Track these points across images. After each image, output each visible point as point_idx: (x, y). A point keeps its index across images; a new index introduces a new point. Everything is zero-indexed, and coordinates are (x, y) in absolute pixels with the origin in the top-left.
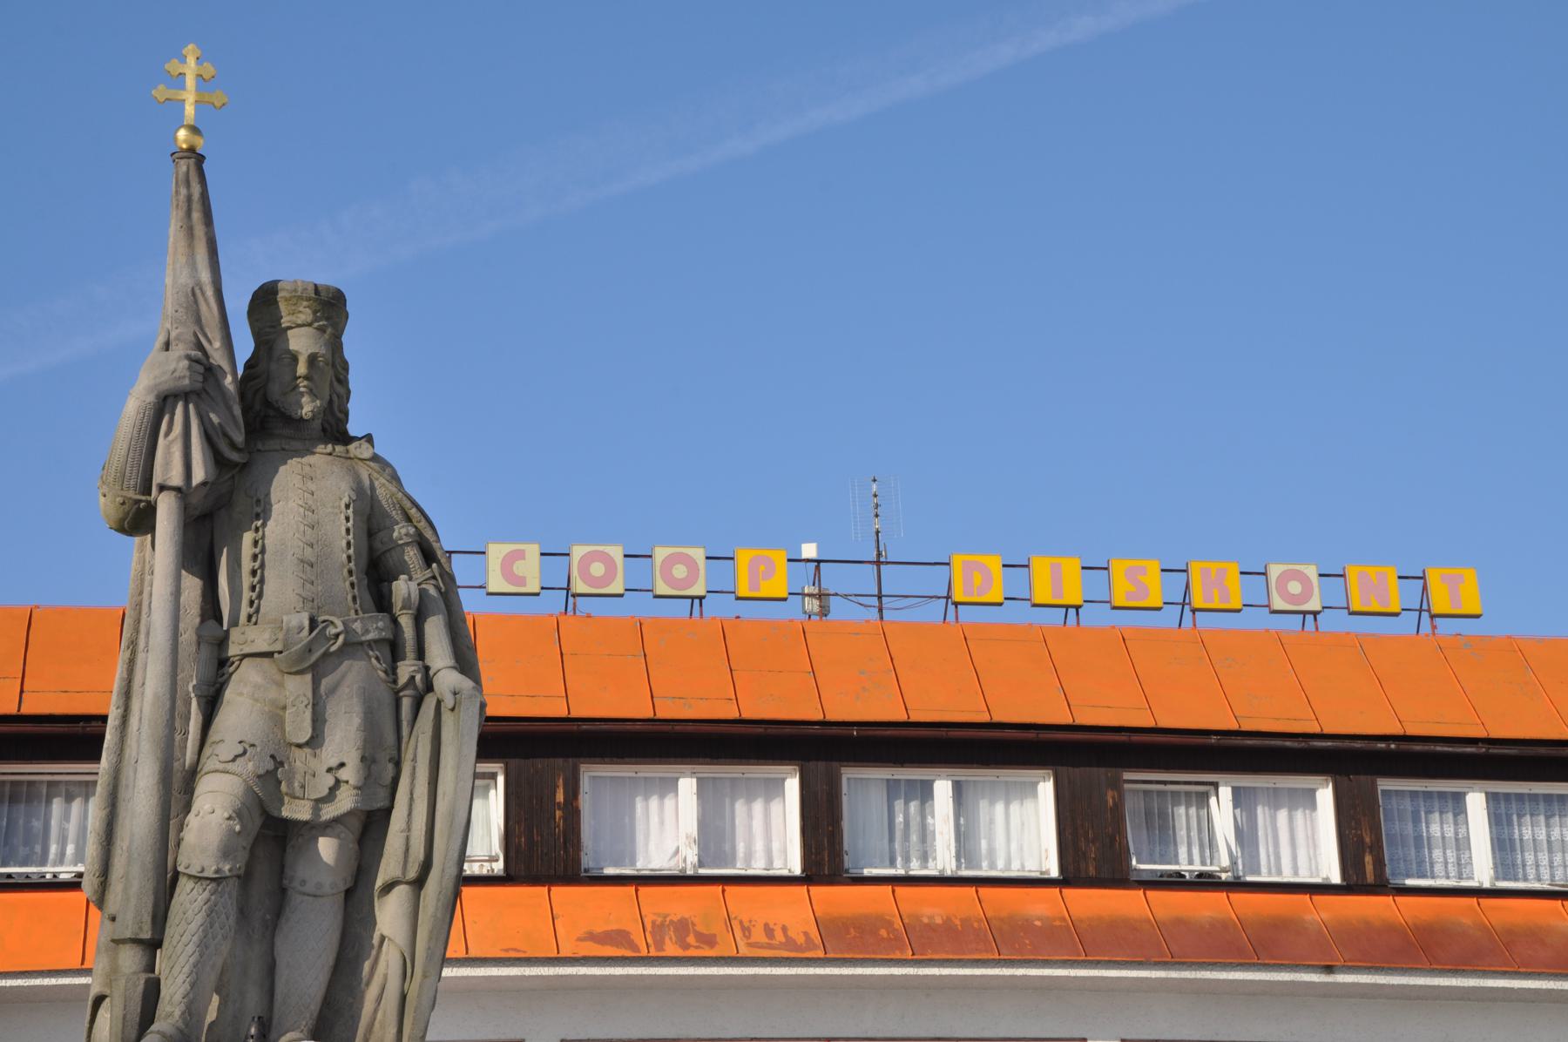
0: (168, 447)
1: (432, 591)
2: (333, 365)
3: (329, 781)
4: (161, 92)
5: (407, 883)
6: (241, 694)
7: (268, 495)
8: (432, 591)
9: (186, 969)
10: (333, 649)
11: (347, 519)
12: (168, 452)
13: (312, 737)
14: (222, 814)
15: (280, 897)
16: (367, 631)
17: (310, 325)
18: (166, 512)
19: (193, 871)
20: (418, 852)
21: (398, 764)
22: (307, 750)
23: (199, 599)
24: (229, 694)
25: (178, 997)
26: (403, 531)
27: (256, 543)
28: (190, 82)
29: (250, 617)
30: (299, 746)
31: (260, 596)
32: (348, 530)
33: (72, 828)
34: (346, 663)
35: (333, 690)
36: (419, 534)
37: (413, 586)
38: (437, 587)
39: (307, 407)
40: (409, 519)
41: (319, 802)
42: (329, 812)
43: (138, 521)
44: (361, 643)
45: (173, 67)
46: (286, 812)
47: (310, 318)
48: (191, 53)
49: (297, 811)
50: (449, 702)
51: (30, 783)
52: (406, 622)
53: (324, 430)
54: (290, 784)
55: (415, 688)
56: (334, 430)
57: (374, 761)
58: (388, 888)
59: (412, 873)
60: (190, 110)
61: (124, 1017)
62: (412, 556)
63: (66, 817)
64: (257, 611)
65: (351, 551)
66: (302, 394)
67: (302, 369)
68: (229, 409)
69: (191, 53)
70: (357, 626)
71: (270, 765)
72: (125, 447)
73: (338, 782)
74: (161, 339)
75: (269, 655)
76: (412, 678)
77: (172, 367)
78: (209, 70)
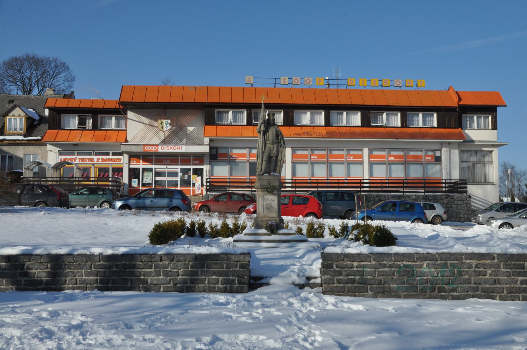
49: (272, 155)
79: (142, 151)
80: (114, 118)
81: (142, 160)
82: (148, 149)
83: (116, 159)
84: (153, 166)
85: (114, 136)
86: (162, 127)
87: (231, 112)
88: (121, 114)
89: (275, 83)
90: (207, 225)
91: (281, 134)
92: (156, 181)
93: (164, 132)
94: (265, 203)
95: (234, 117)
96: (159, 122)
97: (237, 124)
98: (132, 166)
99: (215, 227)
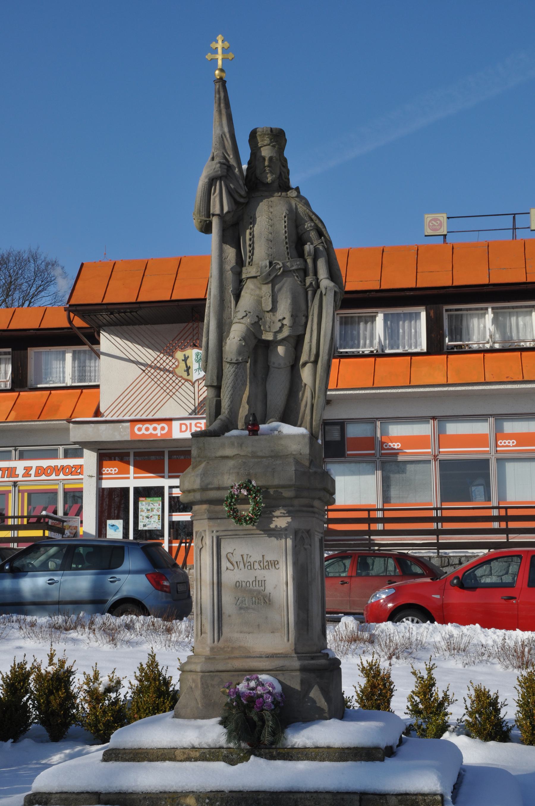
0: (214, 199)
1: (321, 248)
2: (280, 160)
3: (279, 325)
4: (209, 56)
5: (311, 362)
6: (246, 293)
7: (255, 214)
8: (321, 248)
9: (228, 396)
10: (279, 273)
11: (285, 222)
12: (214, 201)
13: (272, 308)
14: (237, 339)
15: (267, 369)
16: (292, 266)
17: (269, 145)
18: (215, 223)
19: (229, 360)
20: (314, 351)
21: (307, 317)
22: (271, 313)
23: (235, 257)
24: (243, 293)
25: (226, 406)
26: (309, 225)
27: (250, 234)
28: (220, 51)
29: (249, 263)
30: (268, 312)
31: (253, 254)
32: (285, 227)
33: (368, 334)
34: (285, 279)
35: (280, 289)
36: (316, 225)
37: (312, 247)
38: (323, 246)
39: (270, 178)
40: (312, 220)
41: (276, 333)
42: (280, 337)
43: (207, 228)
44: (290, 271)
45: (213, 45)
46: (264, 337)
47: (269, 142)
48: (220, 38)
49: (268, 336)
50: (324, 293)
51: (352, 317)
52: (309, 261)
53: (280, 186)
54: (265, 326)
55: (313, 287)
56: (283, 185)
57: (297, 316)
58: (304, 364)
59: (312, 359)
60: (220, 62)
61: (210, 413)
62: (313, 235)
63: (365, 329)
64: (252, 260)
65: (287, 235)
66: (267, 173)
67: (266, 163)
68: (238, 182)
69: (220, 38)
70: (288, 264)
71: (256, 320)
72: (199, 200)
73: (283, 325)
74: (211, 156)
75: (255, 277)
76: (311, 283)
77: (214, 167)
78: (227, 45)
79: (128, 438)
80: (69, 356)
81: (135, 466)
82: (144, 431)
83: (75, 466)
84: (165, 483)
85: (66, 401)
86: (188, 369)
87: (380, 319)
88: (84, 344)
89: (514, 228)
90: (78, 682)
91: (320, 234)
92: (172, 524)
93: (193, 384)
94: (230, 577)
95: (392, 332)
96: (179, 355)
97: (400, 351)
98: (106, 484)
99: (109, 690)
